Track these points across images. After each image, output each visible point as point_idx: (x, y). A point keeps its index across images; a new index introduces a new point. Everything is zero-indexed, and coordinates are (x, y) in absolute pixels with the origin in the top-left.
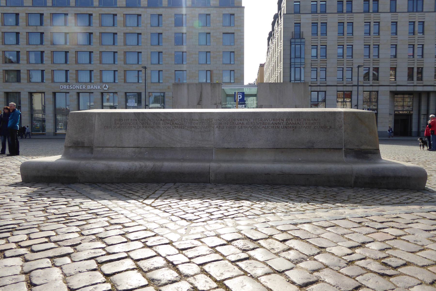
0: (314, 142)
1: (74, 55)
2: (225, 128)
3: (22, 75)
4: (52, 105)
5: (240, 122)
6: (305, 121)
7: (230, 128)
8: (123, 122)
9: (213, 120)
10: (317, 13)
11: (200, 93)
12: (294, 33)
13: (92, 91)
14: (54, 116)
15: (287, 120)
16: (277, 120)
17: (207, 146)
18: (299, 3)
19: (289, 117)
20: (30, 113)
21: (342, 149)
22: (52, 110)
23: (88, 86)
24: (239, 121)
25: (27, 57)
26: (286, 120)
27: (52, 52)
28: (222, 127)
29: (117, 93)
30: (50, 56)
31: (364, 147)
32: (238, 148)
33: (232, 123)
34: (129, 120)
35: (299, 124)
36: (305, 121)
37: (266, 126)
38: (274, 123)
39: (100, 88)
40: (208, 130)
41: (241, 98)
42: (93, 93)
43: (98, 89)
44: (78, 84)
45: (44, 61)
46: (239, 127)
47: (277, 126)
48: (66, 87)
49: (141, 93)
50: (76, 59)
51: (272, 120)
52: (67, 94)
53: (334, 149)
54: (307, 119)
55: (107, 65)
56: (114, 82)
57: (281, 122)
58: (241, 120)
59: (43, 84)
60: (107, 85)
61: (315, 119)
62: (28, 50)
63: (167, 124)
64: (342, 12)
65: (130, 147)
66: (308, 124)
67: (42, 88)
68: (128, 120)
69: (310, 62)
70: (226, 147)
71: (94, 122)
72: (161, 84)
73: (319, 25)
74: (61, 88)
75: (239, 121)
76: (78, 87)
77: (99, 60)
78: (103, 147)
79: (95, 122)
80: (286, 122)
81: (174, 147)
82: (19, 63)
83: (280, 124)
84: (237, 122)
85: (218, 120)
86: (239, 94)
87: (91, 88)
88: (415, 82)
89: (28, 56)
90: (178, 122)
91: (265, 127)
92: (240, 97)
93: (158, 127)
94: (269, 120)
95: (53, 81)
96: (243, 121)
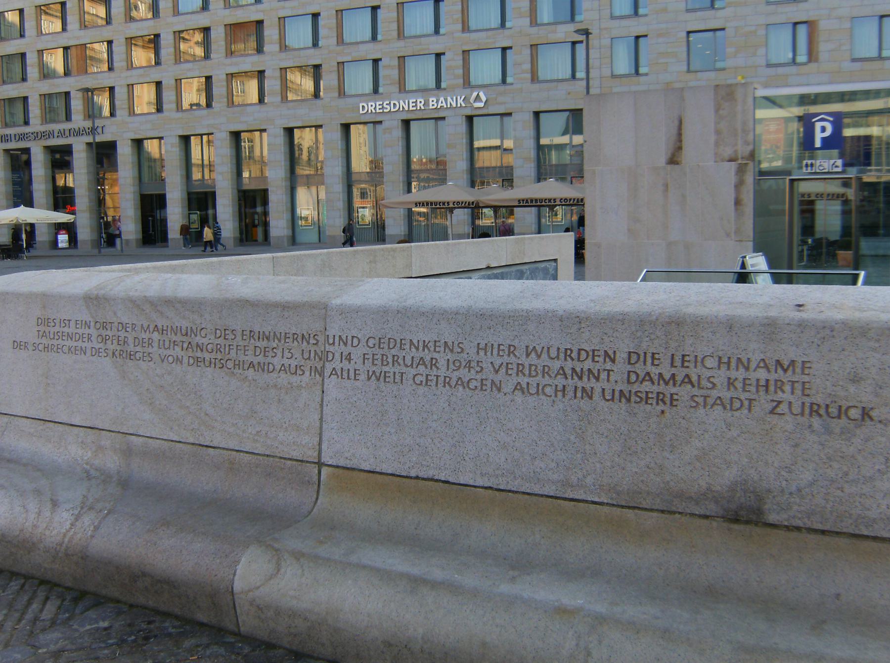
1: (395, 14)
2: (363, 377)
5: (421, 354)
6: (724, 367)
7: (382, 379)
11: (677, 123)
13: (441, 115)
14: (346, 190)
15: (634, 358)
19: (644, 345)
20: (289, 183)
26: (625, 356)
27: (340, 13)
29: (510, 114)
30: (335, 25)
33: (390, 360)
35: (691, 382)
36: (724, 367)
37: (533, 381)
38: (569, 372)
39: (463, 105)
42: (443, 118)
43: (459, 105)
44: (404, 95)
45: (320, 39)
46: (418, 379)
47: (580, 384)
48: (375, 108)
49: (581, 110)
50: (398, 27)
51: (562, 355)
52: (377, 126)
55: (483, 34)
56: (504, 81)
58: (425, 346)
59: (318, 101)
60: (482, 95)
62: (282, 14)
66: (739, 385)
67: (315, 114)
72: (642, 79)
74: (361, 112)
76: (407, 104)
77: (460, 20)
83: (597, 379)
84: (410, 354)
87: (440, 105)
90: (205, 341)
91: (525, 386)
92: (823, 129)
94: (544, 356)
95: (342, 93)
96: (432, 349)
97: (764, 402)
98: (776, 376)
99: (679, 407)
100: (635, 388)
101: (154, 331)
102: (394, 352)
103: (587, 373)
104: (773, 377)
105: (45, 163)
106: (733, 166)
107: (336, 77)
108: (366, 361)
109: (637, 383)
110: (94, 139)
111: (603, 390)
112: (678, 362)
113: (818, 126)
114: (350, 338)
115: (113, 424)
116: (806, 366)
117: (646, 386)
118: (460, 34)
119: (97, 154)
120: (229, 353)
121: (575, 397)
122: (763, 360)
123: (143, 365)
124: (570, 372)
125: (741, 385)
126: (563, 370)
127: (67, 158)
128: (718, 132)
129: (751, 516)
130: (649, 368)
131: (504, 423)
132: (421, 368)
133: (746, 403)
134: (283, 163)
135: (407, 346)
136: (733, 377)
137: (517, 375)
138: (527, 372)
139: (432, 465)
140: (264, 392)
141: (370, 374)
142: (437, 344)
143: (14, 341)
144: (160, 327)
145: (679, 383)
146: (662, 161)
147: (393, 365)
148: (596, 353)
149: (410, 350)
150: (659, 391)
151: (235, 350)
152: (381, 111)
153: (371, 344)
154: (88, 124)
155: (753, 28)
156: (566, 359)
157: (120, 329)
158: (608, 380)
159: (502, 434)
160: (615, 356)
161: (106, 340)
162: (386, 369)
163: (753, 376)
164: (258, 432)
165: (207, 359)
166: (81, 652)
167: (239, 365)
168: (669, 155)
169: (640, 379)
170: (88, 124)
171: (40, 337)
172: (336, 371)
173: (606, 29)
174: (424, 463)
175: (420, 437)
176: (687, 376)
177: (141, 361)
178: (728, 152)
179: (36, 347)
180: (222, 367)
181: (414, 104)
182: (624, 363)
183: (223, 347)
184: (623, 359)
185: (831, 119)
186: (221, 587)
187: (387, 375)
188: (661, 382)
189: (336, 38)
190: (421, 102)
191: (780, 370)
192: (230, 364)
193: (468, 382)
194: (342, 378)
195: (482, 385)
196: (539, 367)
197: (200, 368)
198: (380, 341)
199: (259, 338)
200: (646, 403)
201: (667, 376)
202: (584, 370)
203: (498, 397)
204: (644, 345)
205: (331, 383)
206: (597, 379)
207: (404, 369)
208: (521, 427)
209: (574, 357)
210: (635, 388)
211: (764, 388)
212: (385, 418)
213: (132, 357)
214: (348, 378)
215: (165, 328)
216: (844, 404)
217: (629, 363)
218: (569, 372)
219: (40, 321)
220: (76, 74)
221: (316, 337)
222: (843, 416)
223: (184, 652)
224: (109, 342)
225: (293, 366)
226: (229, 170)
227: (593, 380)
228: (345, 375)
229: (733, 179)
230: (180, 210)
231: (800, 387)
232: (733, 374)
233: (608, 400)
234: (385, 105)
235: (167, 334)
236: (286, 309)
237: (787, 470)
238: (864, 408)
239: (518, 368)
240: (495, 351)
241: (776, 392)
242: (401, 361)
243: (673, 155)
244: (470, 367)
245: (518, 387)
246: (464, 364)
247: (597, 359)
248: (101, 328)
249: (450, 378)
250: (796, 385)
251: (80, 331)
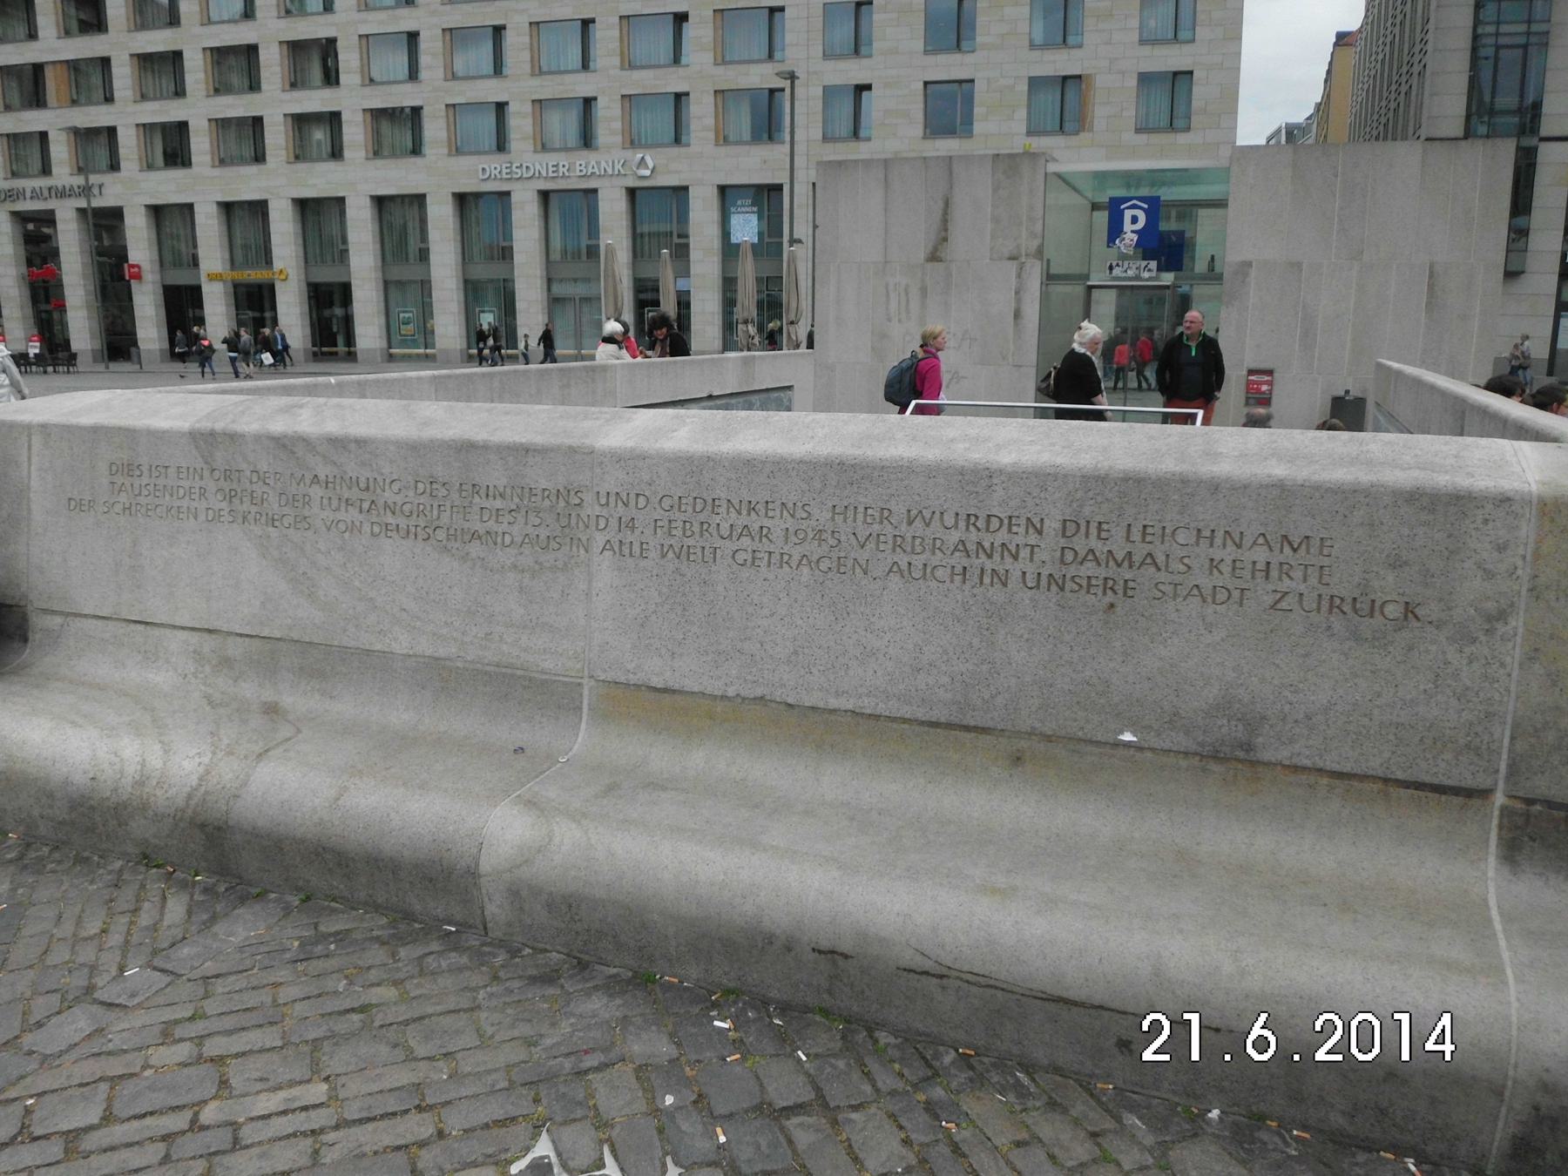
0: (1264, 718)
2: (654, 554)
3: (345, 129)
4: (452, 242)
6: (1204, 543)
8: (145, 480)
9: (588, 497)
11: (941, 204)
15: (1071, 528)
16: (995, 523)
17: (548, 664)
19: (1087, 511)
20: (380, 275)
21: (1485, 793)
22: (453, 263)
23: (578, 164)
24: (739, 513)
25: (361, 59)
26: (1058, 525)
27: (448, 33)
28: (636, 548)
32: (724, 697)
33: (696, 528)
34: (169, 470)
36: (1204, 543)
37: (918, 561)
38: (972, 547)
40: (560, 564)
41: (1141, 224)
43: (616, 172)
46: (740, 557)
50: (532, 57)
51: (962, 524)
53: (1419, 786)
54: (1220, 534)
57: (1020, 540)
58: (752, 509)
61: (1285, 537)
62: (365, 30)
63: (343, 509)
65: (175, 627)
66: (1226, 568)
68: (163, 471)
70: (657, 682)
71: (25, 473)
74: (481, 177)
75: (739, 513)
77: (618, 52)
78: (68, 615)
79: (29, 472)
80: (1063, 542)
81: (378, 647)
82: (417, 78)
83: (1015, 557)
84: (725, 520)
85: (612, 499)
86: (1134, 207)
89: (365, 56)
90: (399, 499)
91: (904, 566)
92: (1134, 220)
93: (302, 522)
94: (936, 523)
97: (1263, 594)
98: (1282, 558)
99: (1135, 599)
100: (1072, 571)
101: (312, 482)
102: (702, 517)
103: (1000, 549)
104: (1276, 559)
105: (13, 236)
107: (445, 126)
108: (658, 530)
109: (1074, 565)
110: (89, 202)
111: (1024, 573)
112: (1136, 535)
113: (1128, 214)
114: (632, 496)
115: (247, 625)
116: (1326, 544)
117: (1088, 569)
118: (618, 72)
119: (95, 225)
120: (439, 517)
121: (981, 583)
122: (1263, 535)
124: (974, 547)
125: (1230, 569)
126: (964, 545)
127: (46, 230)
128: (996, 220)
129: (1237, 753)
130: (1093, 542)
131: (872, 620)
132: (746, 541)
133: (1236, 594)
134: (371, 247)
135: (723, 510)
136: (1217, 558)
137: (894, 550)
138: (909, 549)
139: (761, 680)
140: (496, 576)
141: (665, 550)
142: (771, 506)
143: (70, 499)
144: (322, 477)
145: (1137, 564)
147: (702, 536)
148: (1014, 522)
149: (728, 514)
150: (1108, 576)
151: (448, 513)
152: (509, 176)
153: (666, 503)
154: (79, 181)
156: (967, 529)
157: (255, 480)
158: (1031, 560)
159: (869, 635)
160: (1042, 527)
161: (231, 497)
162: (691, 542)
163: (1248, 556)
164: (486, 634)
165: (403, 526)
166: (1037, 1079)
167: (455, 535)
169: (1079, 560)
170: (79, 181)
171: (116, 493)
172: (611, 545)
173: (815, 73)
174: (749, 677)
175: (741, 640)
176: (1150, 554)
177: (292, 529)
180: (428, 539)
181: (555, 169)
182: (1056, 536)
183: (429, 508)
184: (1054, 530)
185: (1146, 206)
186: (458, 867)
187: (691, 551)
188: (1111, 563)
189: (442, 69)
190: (564, 166)
191: (1287, 549)
192: (441, 534)
193: (818, 561)
194: (621, 554)
195: (839, 565)
196: (927, 541)
197: (391, 540)
198: (680, 502)
199: (487, 495)
200: (1088, 592)
201: (1120, 556)
202: (995, 545)
203: (863, 583)
204: (1087, 511)
206: (1015, 557)
207: (718, 543)
208: (898, 626)
209: (980, 526)
210: (1072, 571)
211: (1264, 573)
212: (687, 613)
213: (276, 523)
214: (631, 555)
215: (331, 480)
216: (1380, 597)
217: (1064, 535)
218: (972, 547)
219: (114, 468)
220: (55, 105)
221: (579, 494)
222: (1377, 614)
223: (406, 965)
224: (236, 501)
225: (543, 537)
226: (294, 254)
227: (1009, 560)
228: (626, 551)
230: (224, 308)
231: (1317, 574)
232: (1218, 554)
233: (1031, 588)
234: (514, 169)
235: (334, 489)
236: (530, 453)
237: (1292, 689)
238: (1407, 603)
239: (895, 542)
240: (860, 517)
241: (1280, 579)
242: (713, 529)
243: (935, 249)
244: (820, 540)
245: (894, 568)
246: (811, 535)
247: (1015, 529)
248: (222, 479)
249: (790, 556)
250: (1310, 570)
251: (186, 484)
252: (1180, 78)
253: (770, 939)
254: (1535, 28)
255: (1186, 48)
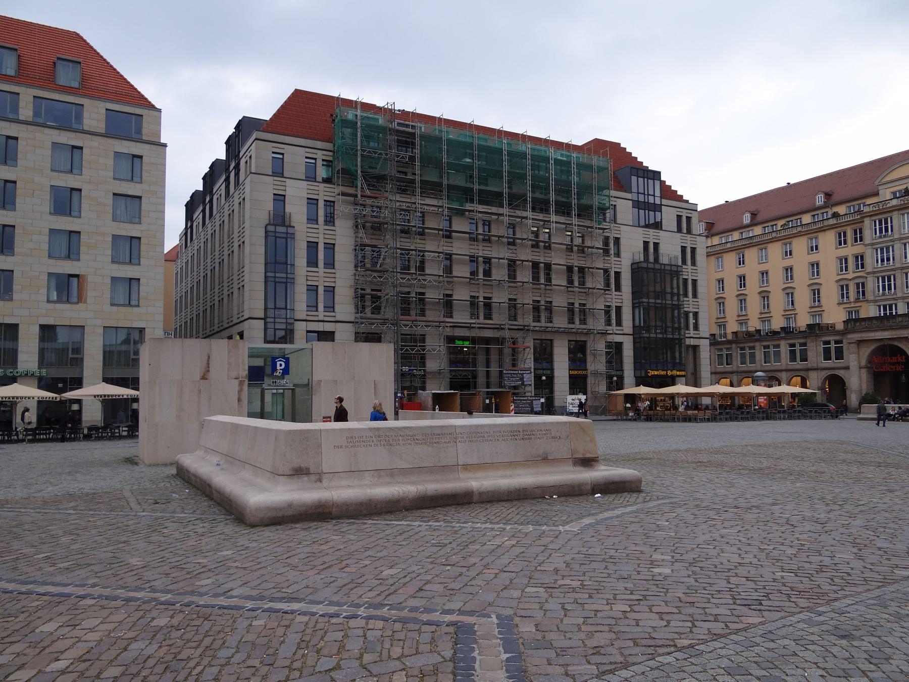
10: (315, 181)
11: (207, 357)
12: (272, 213)
18: (281, 156)
31: (588, 455)
64: (314, 179)
69: (306, 273)
73: (321, 204)
88: (321, 314)
92: (281, 365)
106: (237, 382)
113: (278, 363)
123: (397, 447)
128: (229, 364)
146: (198, 377)
155: (37, 274)
168: (202, 375)
178: (234, 374)
179: (346, 447)
205: (459, 444)
229: (237, 388)
243: (204, 374)
252: (133, 282)
253: (511, 492)
254: (289, 276)
255: (136, 268)
